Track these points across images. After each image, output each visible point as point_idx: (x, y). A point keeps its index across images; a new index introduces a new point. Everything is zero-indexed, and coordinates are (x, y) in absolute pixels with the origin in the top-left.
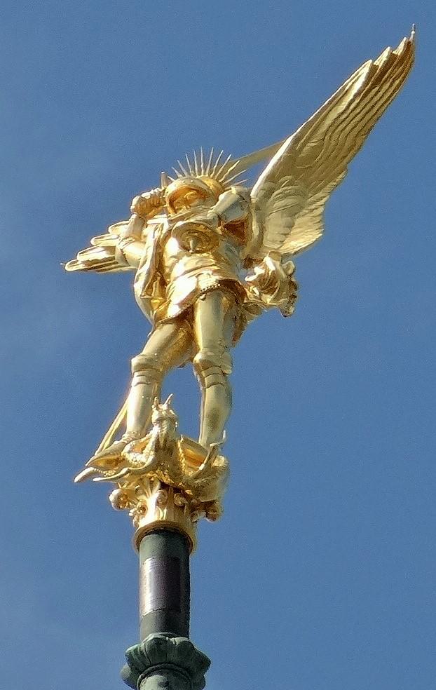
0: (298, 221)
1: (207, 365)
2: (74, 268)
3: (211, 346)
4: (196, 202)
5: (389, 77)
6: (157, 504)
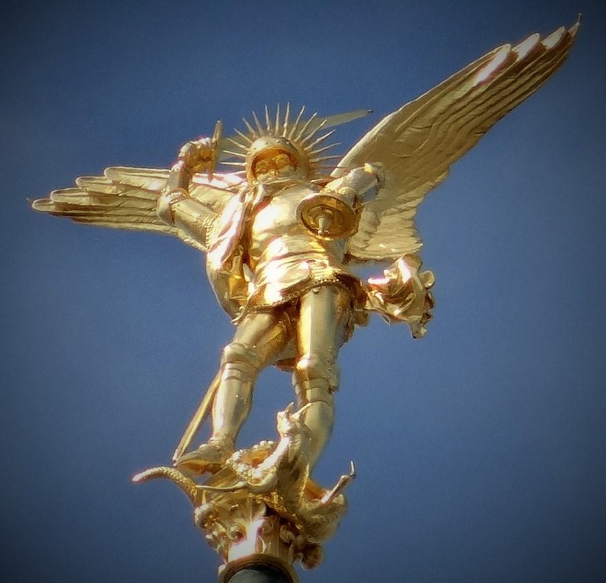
0: (385, 220)
1: (312, 374)
2: (44, 209)
3: (318, 351)
4: (287, 169)
5: (530, 70)
6: (260, 531)
